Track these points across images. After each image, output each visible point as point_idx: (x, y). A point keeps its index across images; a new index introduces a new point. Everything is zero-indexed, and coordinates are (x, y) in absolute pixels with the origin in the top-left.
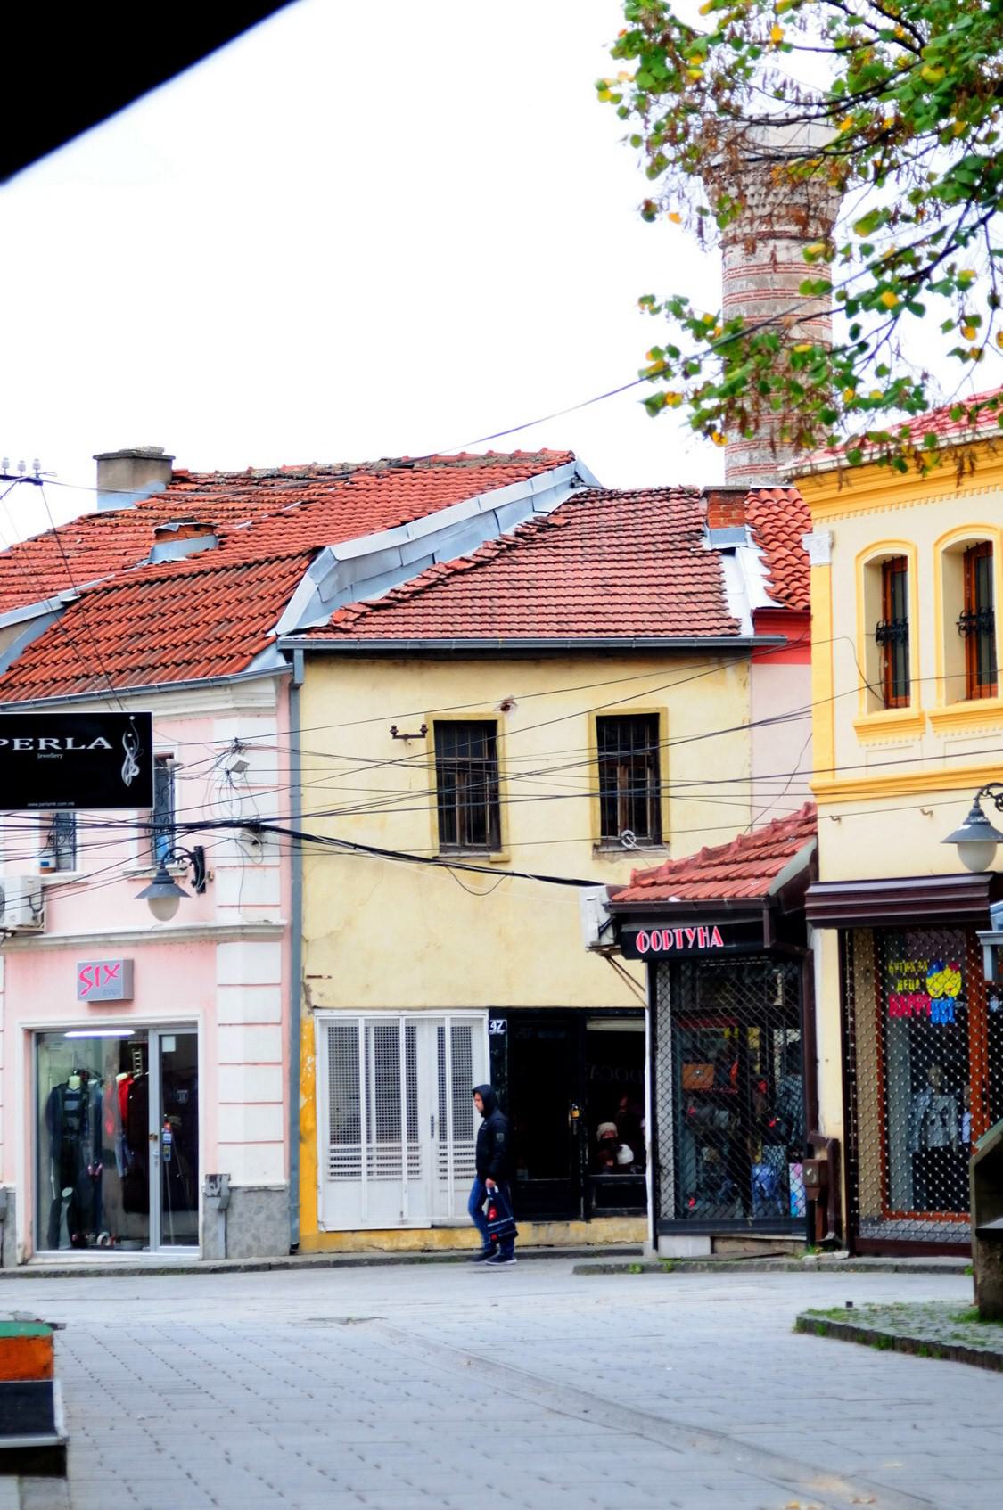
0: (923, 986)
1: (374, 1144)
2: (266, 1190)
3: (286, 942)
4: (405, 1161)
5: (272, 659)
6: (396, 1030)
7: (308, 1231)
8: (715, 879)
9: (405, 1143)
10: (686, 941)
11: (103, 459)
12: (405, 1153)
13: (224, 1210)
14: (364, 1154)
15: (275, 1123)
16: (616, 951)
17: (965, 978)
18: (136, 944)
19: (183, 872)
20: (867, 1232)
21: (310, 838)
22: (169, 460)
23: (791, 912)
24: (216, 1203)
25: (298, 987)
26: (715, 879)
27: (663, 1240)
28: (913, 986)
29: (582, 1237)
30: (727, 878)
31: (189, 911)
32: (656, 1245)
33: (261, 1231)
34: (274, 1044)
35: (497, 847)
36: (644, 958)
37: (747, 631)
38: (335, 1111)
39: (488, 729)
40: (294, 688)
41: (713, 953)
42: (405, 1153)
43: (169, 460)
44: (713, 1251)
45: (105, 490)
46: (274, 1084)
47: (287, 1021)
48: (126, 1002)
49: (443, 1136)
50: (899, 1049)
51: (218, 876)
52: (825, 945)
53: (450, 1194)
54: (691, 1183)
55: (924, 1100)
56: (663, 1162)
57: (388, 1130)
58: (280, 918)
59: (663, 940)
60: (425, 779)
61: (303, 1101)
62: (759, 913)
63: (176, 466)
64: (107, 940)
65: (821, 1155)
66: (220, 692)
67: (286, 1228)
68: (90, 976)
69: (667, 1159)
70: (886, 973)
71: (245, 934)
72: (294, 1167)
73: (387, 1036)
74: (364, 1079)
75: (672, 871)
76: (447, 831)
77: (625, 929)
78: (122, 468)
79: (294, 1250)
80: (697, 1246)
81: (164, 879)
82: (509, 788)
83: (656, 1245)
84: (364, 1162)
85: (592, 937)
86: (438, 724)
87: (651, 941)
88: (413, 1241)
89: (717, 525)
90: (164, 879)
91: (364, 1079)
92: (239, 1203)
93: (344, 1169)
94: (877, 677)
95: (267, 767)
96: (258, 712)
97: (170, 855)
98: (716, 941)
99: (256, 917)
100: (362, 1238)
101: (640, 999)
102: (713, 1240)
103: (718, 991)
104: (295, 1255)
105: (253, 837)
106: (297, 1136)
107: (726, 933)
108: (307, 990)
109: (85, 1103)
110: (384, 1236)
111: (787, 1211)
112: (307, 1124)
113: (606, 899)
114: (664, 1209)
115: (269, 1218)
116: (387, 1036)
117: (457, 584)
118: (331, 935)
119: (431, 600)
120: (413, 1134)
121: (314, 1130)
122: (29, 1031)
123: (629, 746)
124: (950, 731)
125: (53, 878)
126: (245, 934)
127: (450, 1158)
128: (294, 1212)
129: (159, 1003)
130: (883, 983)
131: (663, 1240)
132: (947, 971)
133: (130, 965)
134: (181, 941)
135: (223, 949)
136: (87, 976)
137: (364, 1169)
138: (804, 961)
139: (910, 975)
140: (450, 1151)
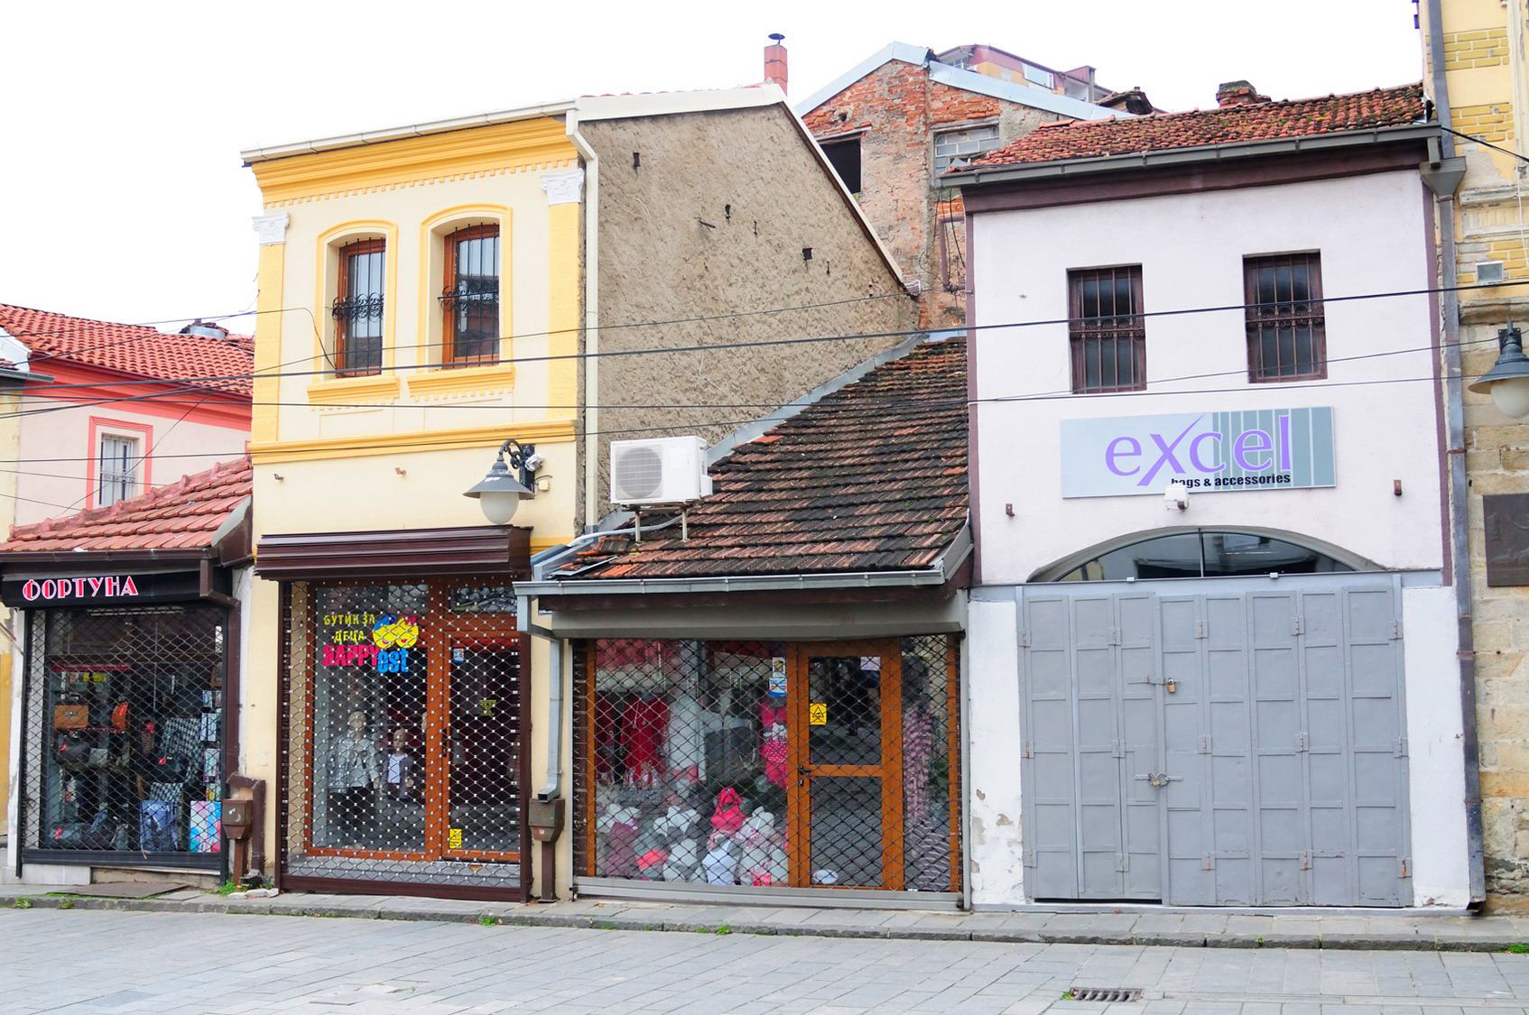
8: (119, 534)
20: (295, 870)
23: (230, 558)
26: (119, 534)
27: (27, 868)
30: (134, 533)
32: (19, 873)
37: (24, 368)
41: (127, 602)
44: (93, 882)
52: (258, 600)
54: (55, 814)
62: (197, 562)
75: (52, 529)
80: (75, 876)
83: (19, 873)
98: (129, 590)
102: (93, 870)
103: (114, 639)
107: (140, 582)
131: (27, 868)
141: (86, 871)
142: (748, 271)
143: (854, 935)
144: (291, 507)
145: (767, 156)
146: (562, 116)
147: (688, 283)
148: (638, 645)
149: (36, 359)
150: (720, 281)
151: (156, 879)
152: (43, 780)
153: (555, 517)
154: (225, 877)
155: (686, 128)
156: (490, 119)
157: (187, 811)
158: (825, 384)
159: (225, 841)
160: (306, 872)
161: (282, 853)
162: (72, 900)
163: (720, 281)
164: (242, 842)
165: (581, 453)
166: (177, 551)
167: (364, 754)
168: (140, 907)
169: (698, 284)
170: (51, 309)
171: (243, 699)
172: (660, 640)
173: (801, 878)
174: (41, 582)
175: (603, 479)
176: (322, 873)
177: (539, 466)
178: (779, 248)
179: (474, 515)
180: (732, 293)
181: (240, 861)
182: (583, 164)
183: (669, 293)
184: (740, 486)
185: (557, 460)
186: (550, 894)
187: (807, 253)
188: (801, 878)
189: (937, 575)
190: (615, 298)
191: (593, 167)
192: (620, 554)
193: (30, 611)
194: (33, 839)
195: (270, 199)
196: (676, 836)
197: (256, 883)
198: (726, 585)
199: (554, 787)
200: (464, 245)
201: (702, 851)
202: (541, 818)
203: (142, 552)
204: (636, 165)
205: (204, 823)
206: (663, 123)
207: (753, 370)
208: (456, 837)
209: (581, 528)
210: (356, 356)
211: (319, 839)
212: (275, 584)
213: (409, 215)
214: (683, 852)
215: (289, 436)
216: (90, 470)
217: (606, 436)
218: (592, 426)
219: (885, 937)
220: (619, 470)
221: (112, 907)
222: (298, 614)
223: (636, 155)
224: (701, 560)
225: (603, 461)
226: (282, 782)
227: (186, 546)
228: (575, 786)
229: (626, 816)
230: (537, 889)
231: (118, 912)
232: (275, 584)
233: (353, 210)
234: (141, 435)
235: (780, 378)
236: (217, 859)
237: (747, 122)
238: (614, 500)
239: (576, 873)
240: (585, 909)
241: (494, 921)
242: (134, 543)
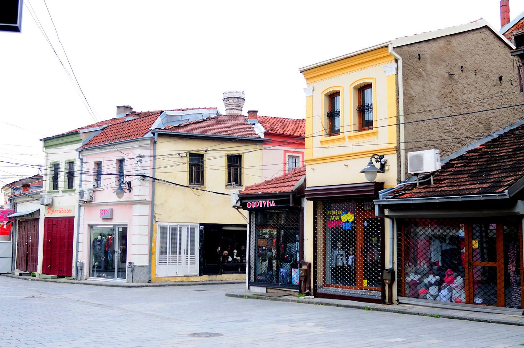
0: (340, 218)
1: (170, 256)
2: (143, 266)
3: (150, 205)
4: (178, 260)
5: (149, 135)
6: (177, 228)
7: (153, 277)
9: (178, 255)
11: (117, 107)
12: (178, 258)
13: (132, 271)
14: (168, 258)
15: (146, 250)
16: (240, 208)
17: (355, 216)
18: (114, 205)
19: (125, 187)
20: (319, 291)
22: (132, 109)
23: (300, 193)
24: (130, 269)
25: (153, 216)
27: (251, 287)
28: (337, 218)
29: (220, 279)
30: (275, 187)
31: (126, 196)
32: (249, 289)
33: (142, 277)
34: (146, 230)
35: (203, 184)
36: (248, 209)
37: (263, 137)
38: (161, 247)
39: (202, 155)
40: (155, 142)
42: (178, 258)
43: (132, 109)
44: (267, 292)
45: (118, 113)
46: (146, 240)
47: (150, 225)
48: (111, 219)
49: (187, 254)
50: (329, 237)
51: (134, 188)
52: (308, 206)
53: (189, 268)
55: (336, 252)
56: (252, 266)
57: (174, 252)
58: (149, 199)
59: (256, 204)
60: (186, 167)
61: (153, 245)
62: (289, 196)
63: (133, 110)
64: (107, 204)
65: (304, 267)
66: (136, 142)
67: (148, 276)
68: (103, 212)
69: (253, 265)
70: (326, 214)
71: (140, 202)
72: (150, 261)
73: (174, 229)
74: (168, 241)
75: (256, 186)
76: (191, 180)
77: (243, 202)
78: (122, 109)
79: (150, 281)
80: (261, 290)
81: (120, 188)
83: (249, 289)
84: (168, 260)
85: (234, 204)
86: (190, 153)
88: (179, 279)
89: (251, 119)
90: (120, 188)
91: (168, 241)
92: (136, 270)
93: (163, 262)
94: (327, 127)
95: (147, 162)
96: (146, 148)
97: (122, 183)
99: (143, 198)
100: (167, 279)
101: (246, 222)
104: (150, 283)
105: (143, 178)
106: (151, 253)
107: (276, 202)
108: (155, 217)
109: (101, 243)
110: (172, 278)
111: (291, 282)
112: (154, 250)
113: (238, 193)
114: (251, 279)
115: (143, 273)
116: (174, 229)
117: (194, 125)
118: (161, 204)
119: (189, 127)
120: (180, 253)
122: (89, 225)
123: (235, 162)
124: (353, 142)
125: (96, 189)
126: (140, 202)
127: (189, 259)
128: (150, 272)
129: (120, 218)
130: (326, 217)
131: (251, 287)
132: (349, 214)
133: (112, 210)
134: (124, 204)
135: (134, 206)
136: (102, 212)
137: (168, 262)
138: (301, 211)
139: (335, 215)
140: (189, 257)
141: (265, 289)
142: (473, 88)
143: (479, 321)
144: (318, 178)
145: (480, 46)
146: (387, 47)
147: (444, 95)
148: (423, 220)
149: (266, 134)
150: (459, 93)
151: (283, 292)
152: (255, 262)
153: (391, 179)
154: (300, 292)
155: (442, 43)
156: (366, 50)
157: (291, 272)
158: (512, 125)
159: (300, 281)
160: (321, 292)
161: (315, 286)
162: (259, 297)
163: (459, 93)
164: (305, 282)
165: (399, 157)
166: (284, 192)
167: (341, 255)
168: (275, 300)
169: (449, 95)
170: (279, 117)
171: (305, 238)
172: (429, 218)
173: (470, 301)
175: (406, 165)
176: (326, 292)
177: (386, 162)
178: (487, 78)
179: (363, 179)
180: (465, 97)
181: (307, 288)
182: (396, 61)
183: (437, 100)
184: (460, 165)
185: (391, 160)
186: (391, 302)
187: (501, 78)
188: (470, 301)
189: (505, 195)
190: (412, 104)
191: (400, 62)
192: (409, 190)
193: (251, 211)
194: (253, 279)
195: (309, 82)
196: (431, 285)
197: (308, 294)
198: (437, 200)
199: (391, 267)
200: (366, 91)
201: (439, 290)
202: (387, 277)
203: (275, 193)
204: (419, 58)
205: (296, 274)
206: (431, 42)
207: (476, 123)
208: (365, 281)
209: (399, 181)
210: (333, 131)
211: (328, 281)
212: (312, 202)
213: (345, 83)
214: (433, 290)
215: (316, 155)
216: (285, 166)
217: (407, 150)
218: (403, 146)
219: (489, 322)
220: (410, 162)
221: (268, 299)
222: (320, 212)
223: (419, 55)
224: (432, 191)
225: (406, 158)
226: (315, 264)
227: (287, 191)
228: (398, 267)
229: (417, 278)
230: (387, 300)
231: (269, 301)
232: (312, 202)
234: (300, 155)
235: (489, 124)
236: (298, 287)
237: (470, 35)
238: (409, 172)
239: (398, 295)
240: (401, 307)
241: (369, 309)
242: (273, 190)
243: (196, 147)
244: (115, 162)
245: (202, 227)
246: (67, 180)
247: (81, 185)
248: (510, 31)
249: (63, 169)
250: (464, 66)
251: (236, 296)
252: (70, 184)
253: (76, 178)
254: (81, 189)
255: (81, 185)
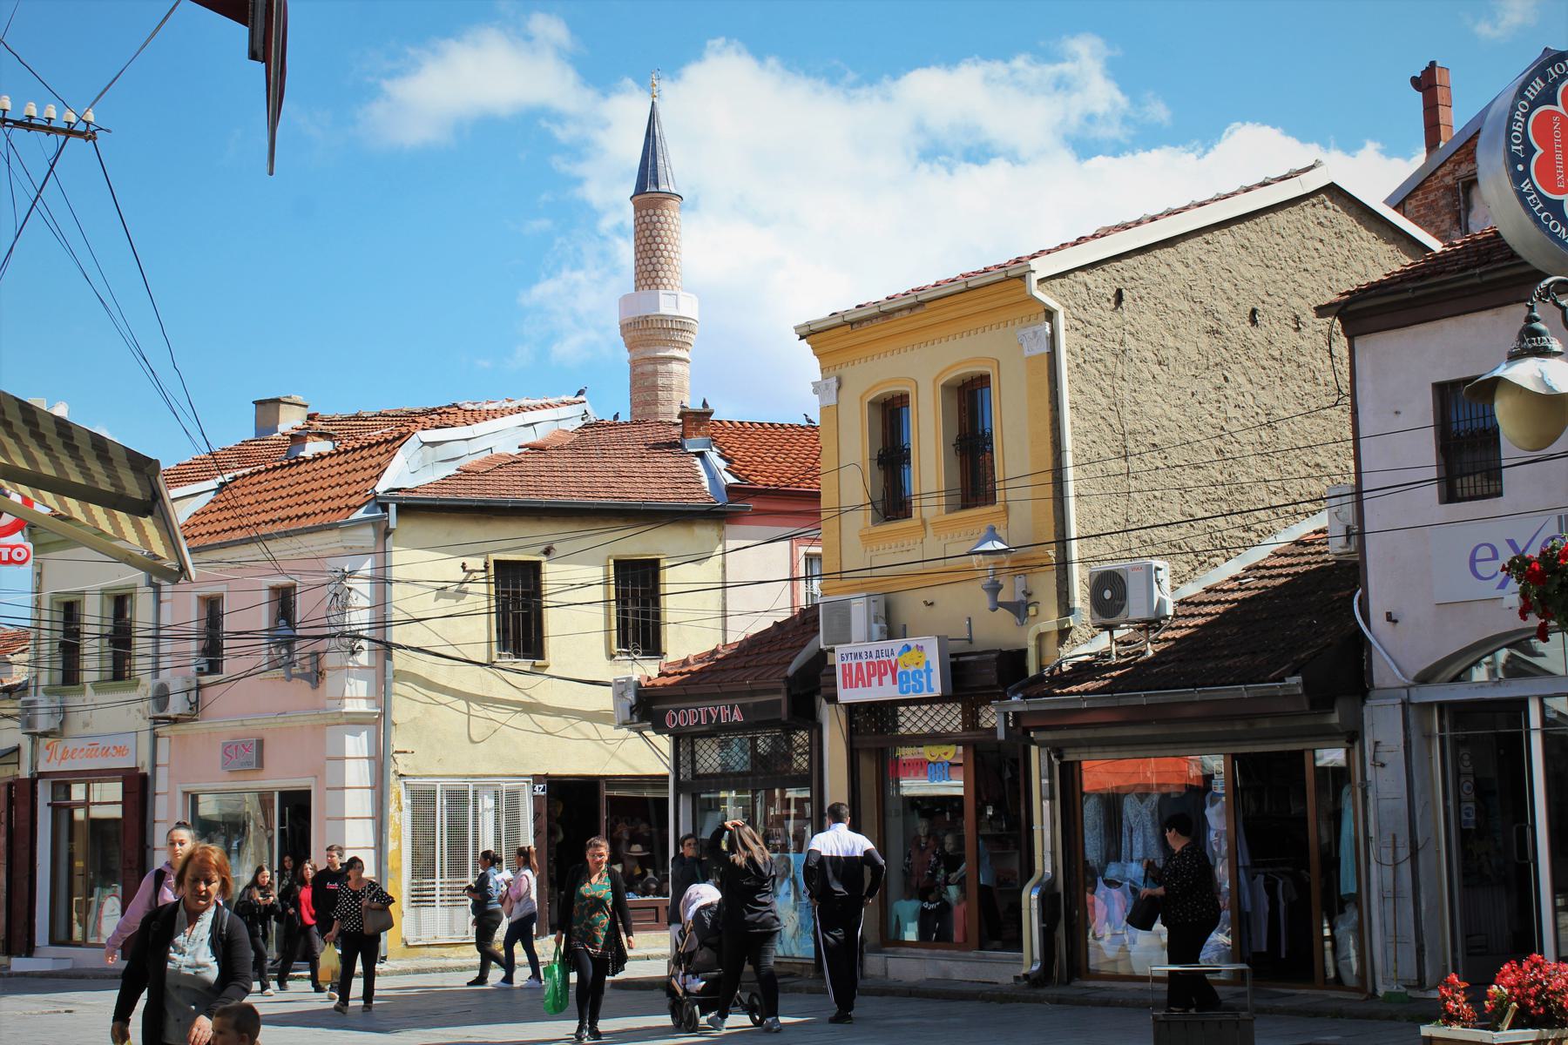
1: (446, 879)
10: (709, 717)
14: (438, 886)
21: (400, 647)
37: (317, 860)
38: (416, 855)
68: (231, 751)
82: (548, 600)
84: (438, 892)
87: (679, 719)
98: (737, 716)
116: (457, 798)
121: (399, 869)
122: (186, 793)
125: (206, 679)
137: (438, 898)
174: (677, 711)
210: (893, 502)
233: (878, 373)
243: (517, 543)
244: (265, 596)
245: (540, 790)
246: (109, 651)
247: (156, 670)
248: (1449, 167)
249: (94, 615)
250: (1260, 307)
251: (153, 35)
252: (120, 672)
253: (142, 645)
254: (158, 681)
255: (156, 670)
